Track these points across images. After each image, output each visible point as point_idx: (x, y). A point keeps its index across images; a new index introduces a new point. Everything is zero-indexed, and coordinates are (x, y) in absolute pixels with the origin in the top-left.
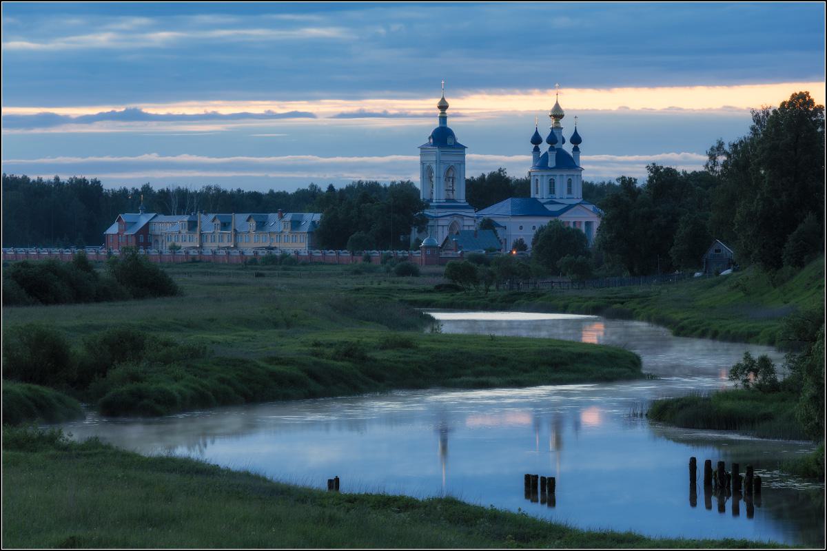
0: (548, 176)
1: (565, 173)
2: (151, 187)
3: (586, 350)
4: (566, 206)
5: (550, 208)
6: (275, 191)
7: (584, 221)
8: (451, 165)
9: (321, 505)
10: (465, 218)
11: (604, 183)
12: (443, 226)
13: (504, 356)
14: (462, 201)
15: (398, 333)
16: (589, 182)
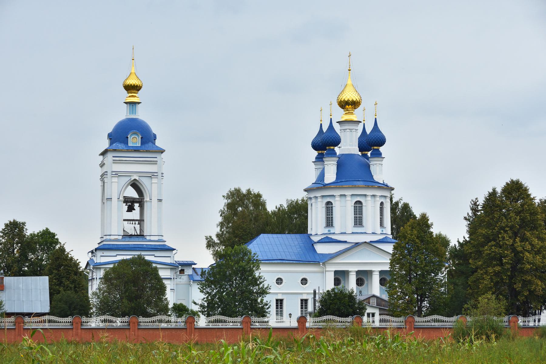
1: (348, 192)
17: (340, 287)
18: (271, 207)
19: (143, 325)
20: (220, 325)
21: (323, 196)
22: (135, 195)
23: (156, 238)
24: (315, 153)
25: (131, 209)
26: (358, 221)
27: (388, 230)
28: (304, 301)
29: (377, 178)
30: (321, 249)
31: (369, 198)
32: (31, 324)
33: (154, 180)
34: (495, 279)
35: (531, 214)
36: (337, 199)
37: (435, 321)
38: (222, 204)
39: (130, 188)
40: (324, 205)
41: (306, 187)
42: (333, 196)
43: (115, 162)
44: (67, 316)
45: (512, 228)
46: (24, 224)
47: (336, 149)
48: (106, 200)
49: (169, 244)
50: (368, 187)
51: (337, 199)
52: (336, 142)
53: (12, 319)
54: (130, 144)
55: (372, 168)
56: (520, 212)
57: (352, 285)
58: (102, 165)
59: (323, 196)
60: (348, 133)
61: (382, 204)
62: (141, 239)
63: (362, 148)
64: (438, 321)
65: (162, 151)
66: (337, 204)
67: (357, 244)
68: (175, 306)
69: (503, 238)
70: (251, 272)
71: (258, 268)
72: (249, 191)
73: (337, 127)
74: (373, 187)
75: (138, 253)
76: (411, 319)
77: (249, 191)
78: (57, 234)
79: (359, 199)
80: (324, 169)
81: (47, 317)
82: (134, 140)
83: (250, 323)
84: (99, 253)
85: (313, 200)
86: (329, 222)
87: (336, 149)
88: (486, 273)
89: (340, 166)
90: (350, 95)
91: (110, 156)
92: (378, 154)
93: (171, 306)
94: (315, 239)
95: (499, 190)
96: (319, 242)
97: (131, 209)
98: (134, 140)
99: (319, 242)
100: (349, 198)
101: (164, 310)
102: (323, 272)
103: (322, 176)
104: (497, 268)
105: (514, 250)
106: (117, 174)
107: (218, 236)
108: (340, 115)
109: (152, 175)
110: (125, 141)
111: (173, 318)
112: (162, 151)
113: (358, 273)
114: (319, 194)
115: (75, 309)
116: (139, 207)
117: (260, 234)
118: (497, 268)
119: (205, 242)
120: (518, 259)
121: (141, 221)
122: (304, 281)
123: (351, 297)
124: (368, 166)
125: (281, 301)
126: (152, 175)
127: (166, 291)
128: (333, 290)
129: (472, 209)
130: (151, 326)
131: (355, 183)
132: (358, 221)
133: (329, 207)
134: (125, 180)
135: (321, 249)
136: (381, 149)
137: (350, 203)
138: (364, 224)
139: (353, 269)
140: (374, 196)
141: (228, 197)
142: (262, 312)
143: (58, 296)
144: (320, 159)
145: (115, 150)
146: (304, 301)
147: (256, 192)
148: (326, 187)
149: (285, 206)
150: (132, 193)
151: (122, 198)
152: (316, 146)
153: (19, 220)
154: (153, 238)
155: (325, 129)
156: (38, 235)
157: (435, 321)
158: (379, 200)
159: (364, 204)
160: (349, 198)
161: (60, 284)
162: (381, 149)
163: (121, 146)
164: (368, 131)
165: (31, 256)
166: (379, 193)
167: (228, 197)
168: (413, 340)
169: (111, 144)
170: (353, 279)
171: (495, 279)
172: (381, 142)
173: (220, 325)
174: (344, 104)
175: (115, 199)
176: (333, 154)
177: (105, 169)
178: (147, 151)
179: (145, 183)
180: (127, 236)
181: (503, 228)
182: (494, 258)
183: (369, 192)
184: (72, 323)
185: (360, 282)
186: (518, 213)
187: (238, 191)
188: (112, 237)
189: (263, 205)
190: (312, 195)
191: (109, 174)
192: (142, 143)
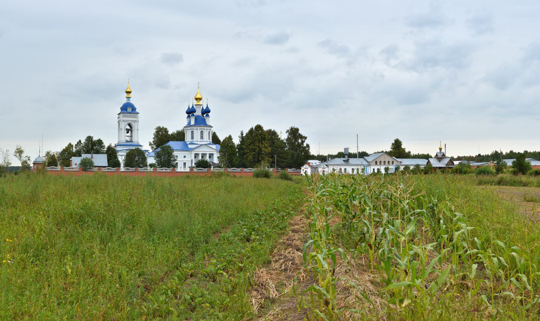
1: (199, 128)
17: (203, 159)
18: (170, 133)
19: (139, 170)
20: (53, 169)
22: (129, 128)
23: (136, 142)
24: (187, 115)
25: (128, 132)
26: (202, 137)
27: (211, 140)
29: (207, 123)
30: (190, 146)
31: (205, 130)
32: (103, 170)
33: (136, 123)
34: (253, 156)
35: (264, 136)
36: (195, 130)
38: (154, 131)
39: (128, 126)
41: (184, 126)
43: (123, 117)
44: (115, 167)
45: (258, 140)
46: (93, 137)
47: (194, 114)
48: (120, 129)
49: (141, 144)
50: (205, 126)
51: (195, 130)
52: (195, 111)
53: (97, 168)
54: (128, 111)
55: (206, 120)
56: (261, 135)
57: (207, 158)
58: (118, 118)
59: (190, 129)
60: (198, 108)
61: (209, 132)
62: (131, 142)
63: (203, 114)
64: (235, 170)
65: (138, 113)
67: (201, 145)
69: (256, 143)
70: (171, 153)
71: (173, 152)
72: (163, 127)
73: (195, 106)
74: (206, 126)
75: (137, 147)
76: (226, 169)
77: (163, 127)
79: (202, 130)
80: (190, 120)
81: (107, 168)
82: (129, 110)
83: (156, 170)
84: (118, 147)
85: (187, 130)
86: (192, 138)
87: (194, 114)
88: (250, 154)
89: (195, 119)
90: (199, 96)
91: (121, 115)
92: (208, 116)
93: (148, 164)
94: (188, 143)
95: (254, 128)
96: (189, 144)
97: (128, 132)
98: (129, 110)
99: (189, 144)
100: (199, 130)
101: (146, 166)
102: (191, 154)
103: (190, 123)
104: (254, 153)
105: (259, 147)
106: (124, 121)
107: (153, 142)
108: (195, 102)
109: (135, 121)
110: (126, 110)
111: (149, 168)
112: (138, 113)
113: (202, 154)
114: (189, 128)
115: (117, 165)
118: (254, 153)
119: (149, 144)
120: (260, 150)
121: (131, 136)
122: (185, 157)
123: (207, 162)
124: (205, 120)
125: (185, 163)
126: (135, 121)
127: (488, 155)
128: (201, 160)
129: (241, 134)
130: (142, 171)
131: (201, 125)
132: (202, 137)
133: (192, 132)
134: (127, 123)
135: (190, 146)
136: (209, 114)
137: (199, 132)
138: (204, 138)
139: (201, 153)
140: (207, 129)
141: (156, 129)
142: (176, 166)
143: (110, 161)
144: (189, 117)
145: (123, 113)
147: (165, 127)
148: (191, 126)
149: (176, 132)
150: (128, 127)
151: (125, 129)
152: (187, 113)
153: (91, 136)
154: (135, 142)
155: (190, 107)
156: (97, 141)
157: (233, 170)
158: (208, 131)
160: (199, 130)
161: (110, 157)
162: (209, 114)
163: (125, 112)
164: (204, 108)
165: (95, 148)
166: (208, 128)
167: (156, 129)
169: (122, 111)
170: (208, 156)
171: (253, 156)
172: (209, 112)
173: (53, 169)
174: (197, 99)
175: (123, 129)
176: (193, 115)
177: (120, 119)
178: (134, 113)
179: (133, 124)
180: (127, 141)
181: (256, 140)
182: (253, 150)
183: (205, 128)
184: (116, 170)
185: (210, 157)
186: (260, 135)
187: (159, 127)
188: (122, 142)
189: (168, 132)
190: (187, 129)
191: (121, 121)
192: (132, 111)
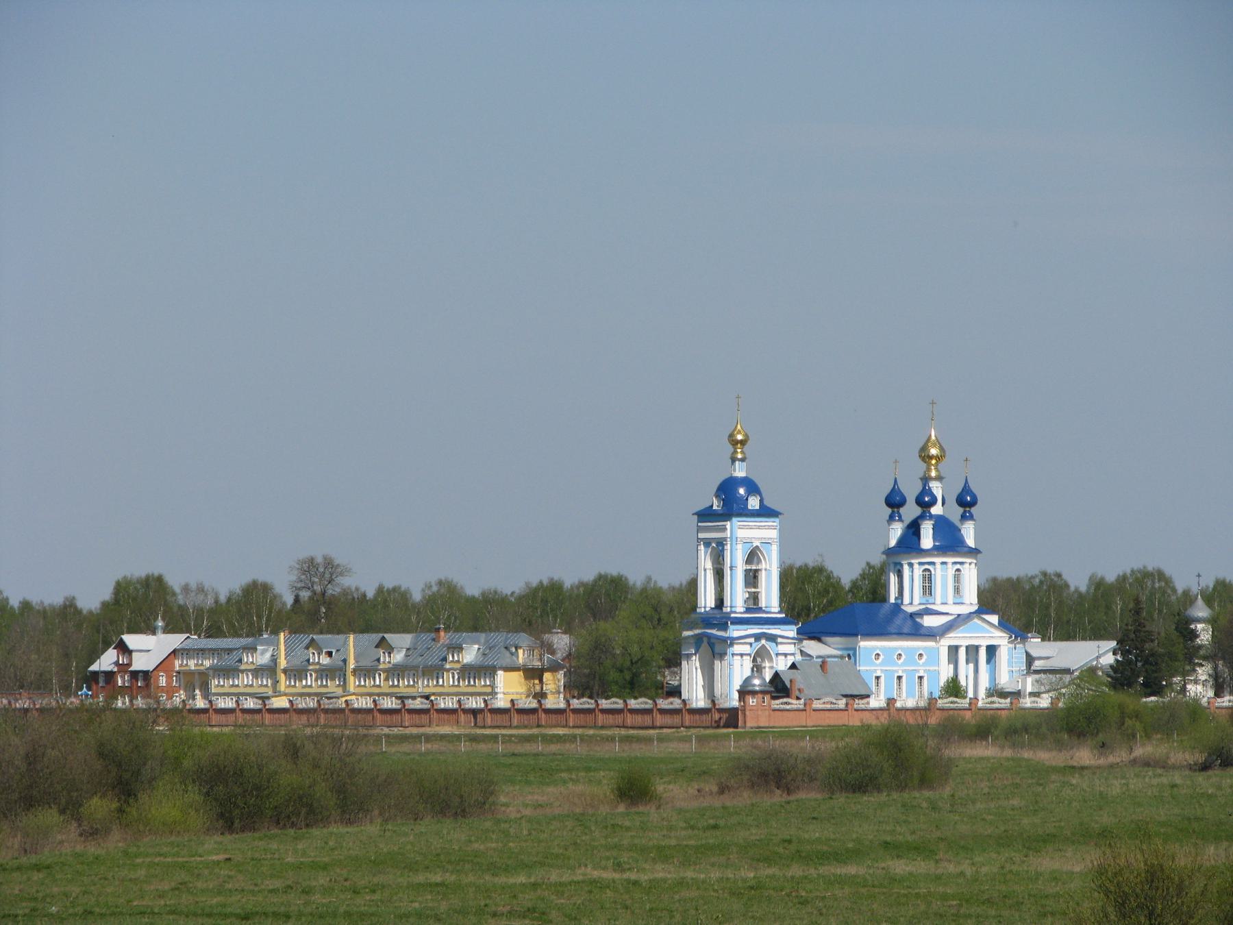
0: (955, 563)
1: (950, 560)
2: (603, 573)
3: (1202, 773)
4: (951, 618)
5: (929, 621)
6: (1111, 577)
7: (984, 643)
8: (755, 545)
9: (1036, 901)
10: (780, 640)
11: (490, 590)
12: (742, 655)
13: (902, 861)
14: (773, 610)
15: (1026, 754)
16: (1015, 577)
21: (921, 564)
28: (197, 676)
37: (952, 703)
40: (921, 573)
42: (933, 563)
66: (938, 572)
68: (22, 614)
72: (380, 590)
78: (821, 555)
79: (927, 567)
86: (928, 589)
116: (116, 650)
117: (926, 627)
137: (951, 571)
140: (943, 563)
146: (197, 676)
159: (933, 572)
168: (476, 703)
